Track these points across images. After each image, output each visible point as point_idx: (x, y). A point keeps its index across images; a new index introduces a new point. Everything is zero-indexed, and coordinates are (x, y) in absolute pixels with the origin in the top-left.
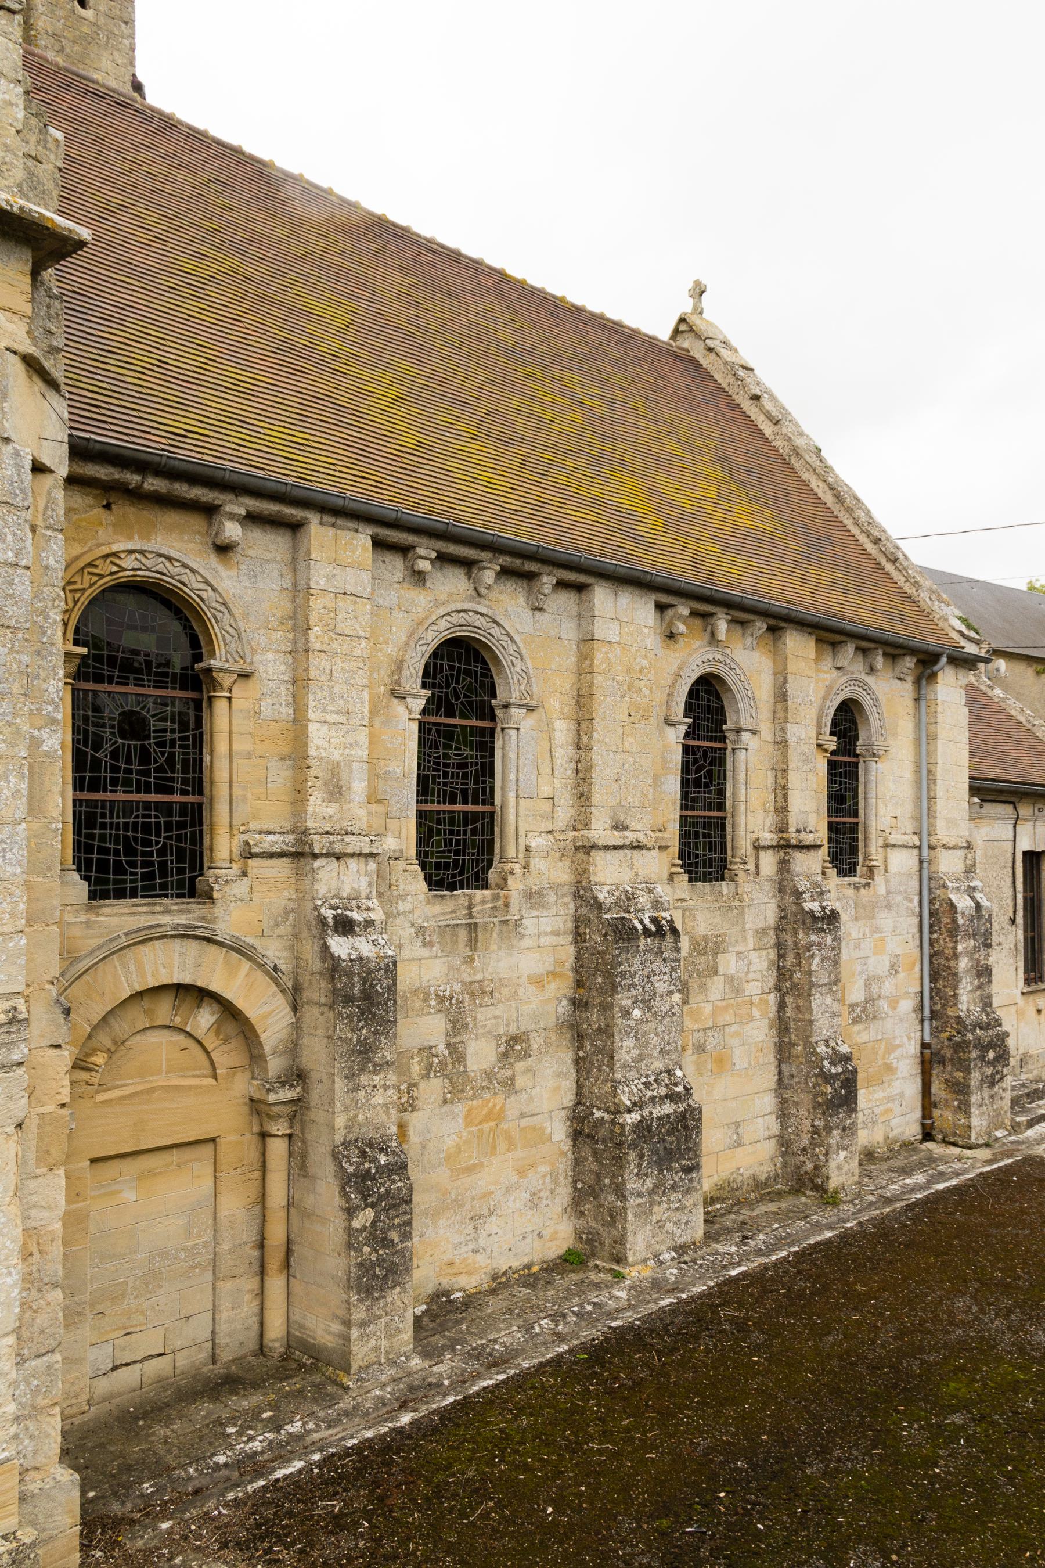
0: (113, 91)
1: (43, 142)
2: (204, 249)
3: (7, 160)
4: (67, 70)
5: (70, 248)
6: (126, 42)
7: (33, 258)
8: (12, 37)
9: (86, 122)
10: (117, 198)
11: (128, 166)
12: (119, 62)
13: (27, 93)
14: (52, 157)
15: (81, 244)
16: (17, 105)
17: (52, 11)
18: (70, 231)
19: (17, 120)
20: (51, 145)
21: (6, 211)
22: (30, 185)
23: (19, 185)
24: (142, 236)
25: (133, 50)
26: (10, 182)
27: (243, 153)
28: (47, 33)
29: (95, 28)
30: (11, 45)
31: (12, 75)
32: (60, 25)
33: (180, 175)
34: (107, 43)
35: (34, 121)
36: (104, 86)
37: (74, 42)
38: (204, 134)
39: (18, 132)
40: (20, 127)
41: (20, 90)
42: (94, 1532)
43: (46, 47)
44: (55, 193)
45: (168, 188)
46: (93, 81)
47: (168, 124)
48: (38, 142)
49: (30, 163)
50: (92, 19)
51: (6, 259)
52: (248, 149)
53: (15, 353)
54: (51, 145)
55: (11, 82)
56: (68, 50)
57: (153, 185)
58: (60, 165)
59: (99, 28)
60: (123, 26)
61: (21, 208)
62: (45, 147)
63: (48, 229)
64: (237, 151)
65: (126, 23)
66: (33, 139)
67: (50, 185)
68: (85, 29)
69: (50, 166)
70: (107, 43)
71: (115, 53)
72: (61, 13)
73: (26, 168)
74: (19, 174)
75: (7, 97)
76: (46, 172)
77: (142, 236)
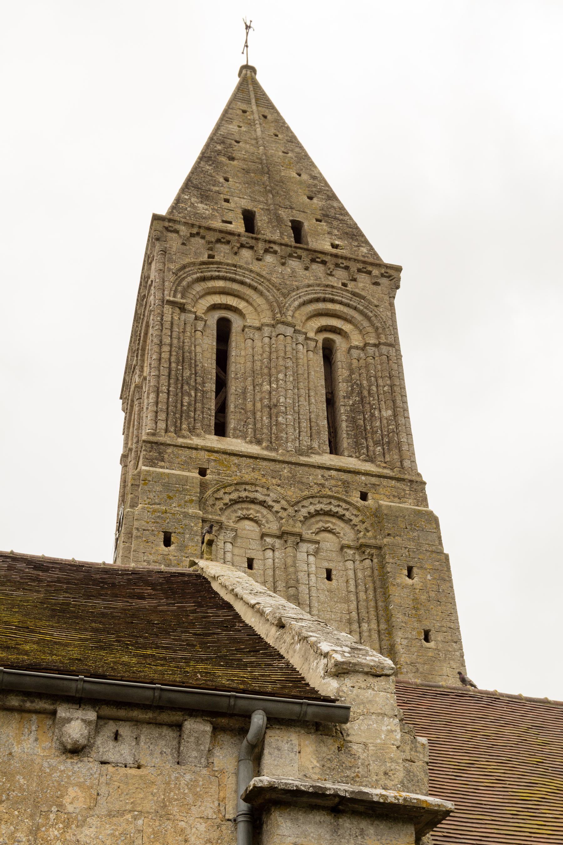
0: (454, 689)
1: (414, 749)
2: (533, 779)
3: (392, 767)
4: (422, 685)
5: (440, 817)
6: (458, 653)
7: (416, 829)
8: (389, 690)
9: (438, 714)
10: (466, 759)
11: (469, 735)
12: (454, 666)
13: (401, 720)
14: (421, 756)
15: (447, 813)
16: (396, 731)
17: (409, 650)
18: (439, 806)
19: (396, 740)
20: (420, 749)
21: (395, 804)
22: (410, 781)
23: (402, 782)
24: (487, 781)
25: (462, 656)
26: (396, 782)
27: (549, 702)
28: (407, 663)
29: (436, 652)
30: (389, 695)
31: (391, 713)
32: (414, 657)
33: (507, 731)
34: (445, 658)
35: (407, 737)
36: (448, 688)
37: (424, 664)
38: (519, 697)
39: (398, 747)
40: (398, 743)
41: (397, 720)
42: (187, 489)
43: (407, 672)
44: (426, 780)
45: (500, 742)
46: (439, 687)
47: (493, 698)
48: (411, 749)
49: (407, 764)
50: (434, 647)
51: (397, 836)
52: (552, 698)
53: (247, 33)
54: (420, 749)
55: (391, 718)
56: (421, 670)
57: (489, 743)
58: (427, 759)
59: (439, 650)
60: (454, 644)
61: (405, 799)
62: (416, 751)
63: (424, 808)
64: (545, 702)
65: (456, 642)
66: (408, 748)
67: (422, 775)
68: (430, 654)
69: (421, 763)
70: (445, 658)
71: (452, 662)
72: (414, 649)
73: (405, 768)
74: (401, 775)
75: (389, 727)
76: (419, 768)
77: (487, 781)
